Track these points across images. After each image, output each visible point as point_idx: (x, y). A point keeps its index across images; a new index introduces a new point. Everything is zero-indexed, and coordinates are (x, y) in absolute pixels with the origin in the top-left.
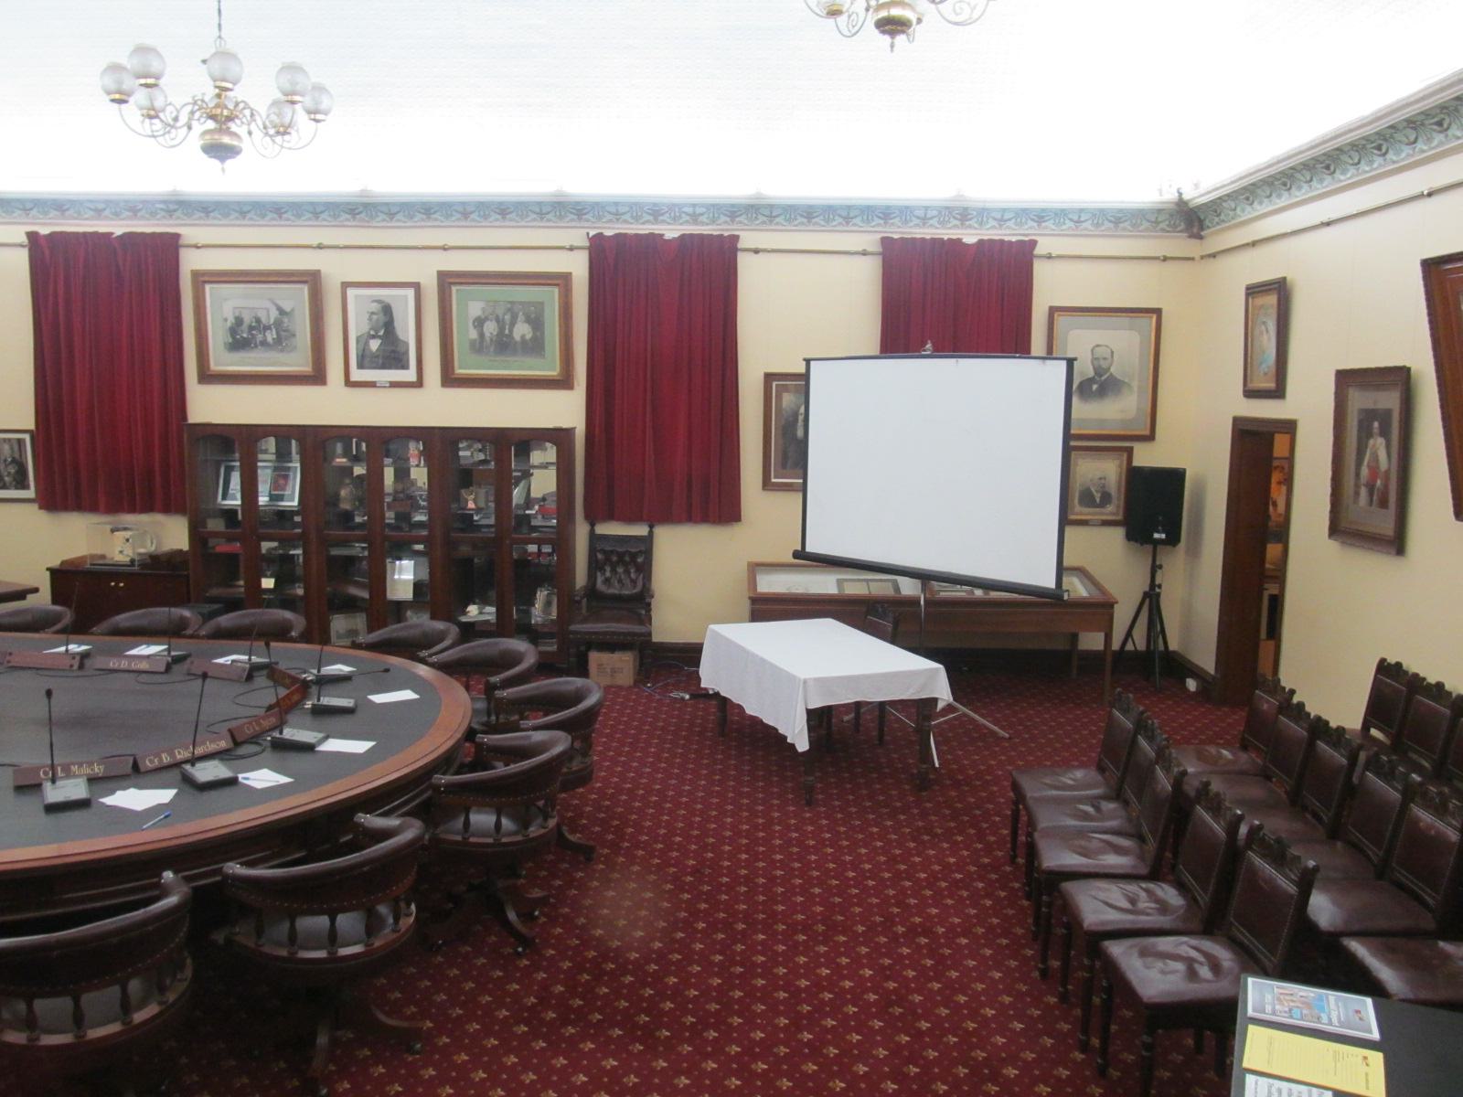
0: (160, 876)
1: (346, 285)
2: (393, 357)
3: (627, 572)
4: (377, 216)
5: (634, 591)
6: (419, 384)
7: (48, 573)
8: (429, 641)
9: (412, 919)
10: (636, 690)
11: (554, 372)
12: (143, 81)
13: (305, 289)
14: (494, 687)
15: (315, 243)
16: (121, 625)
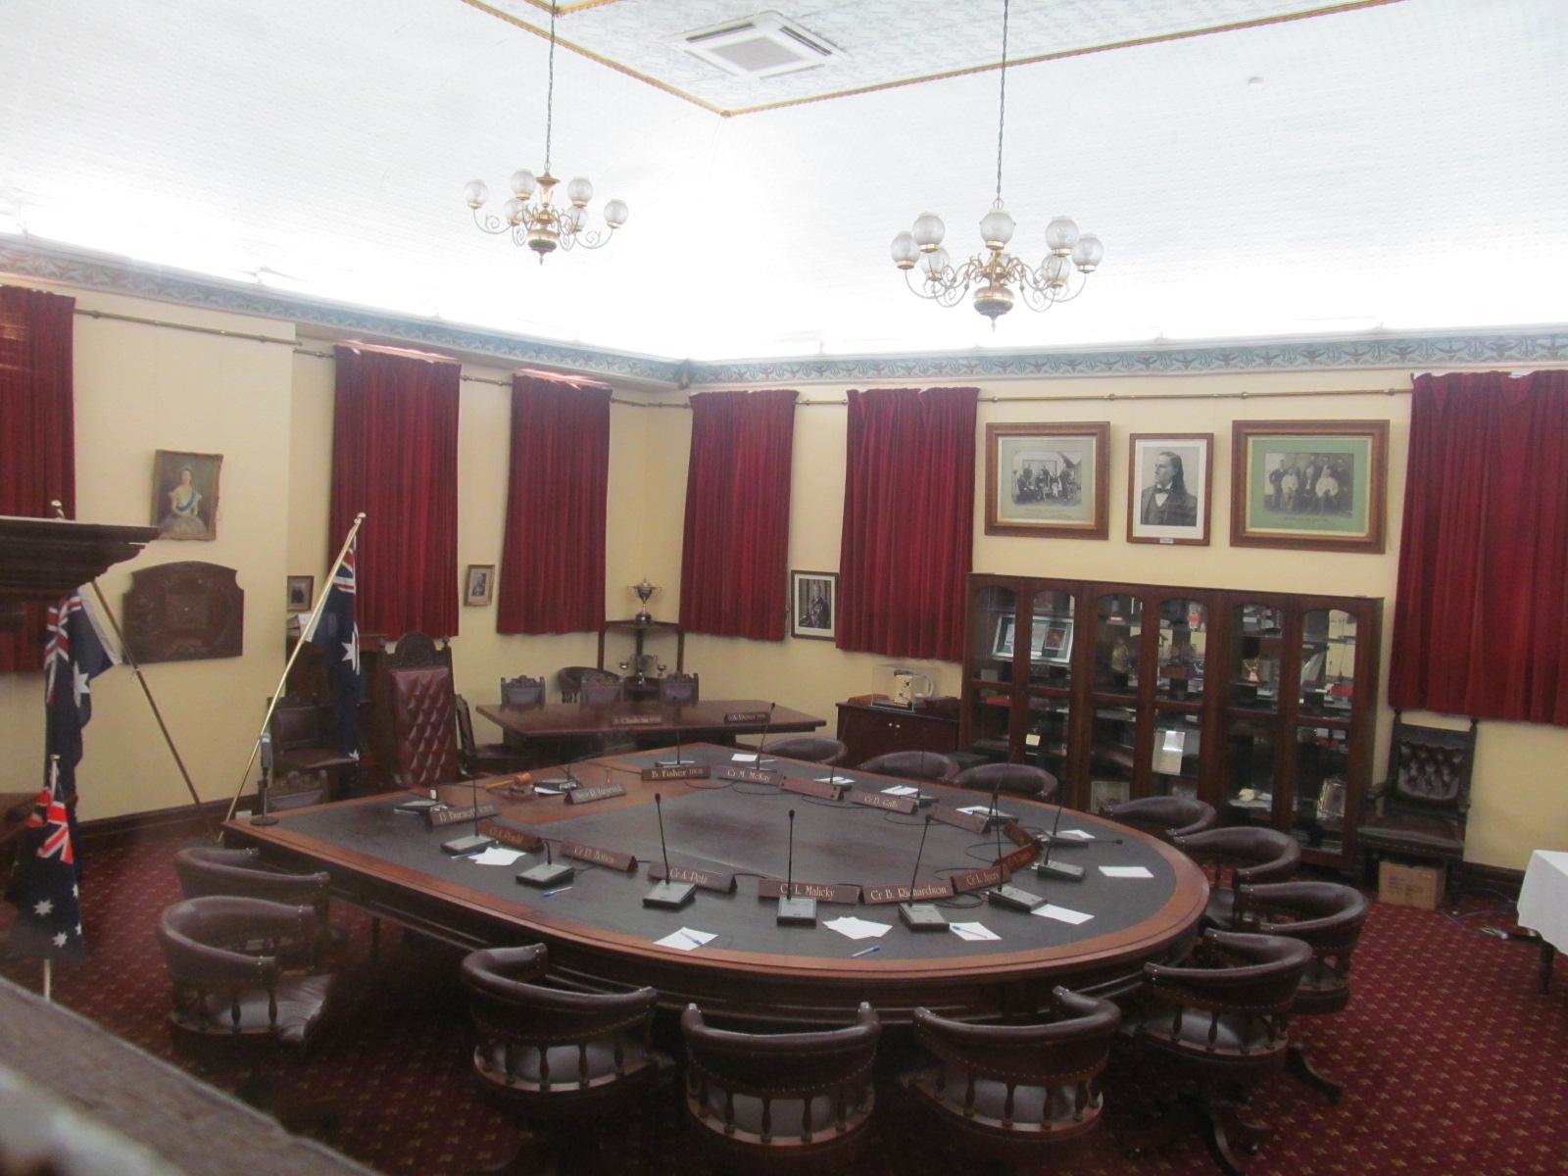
0: (858, 1006)
1: (1134, 437)
2: (1178, 511)
3: (1438, 772)
4: (1173, 365)
5: (1447, 797)
6: (1206, 541)
7: (837, 709)
8: (1182, 819)
9: (1096, 1112)
10: (1437, 916)
11: (1361, 533)
12: (924, 247)
13: (1093, 441)
14: (1243, 880)
15: (1106, 394)
16: (886, 764)
